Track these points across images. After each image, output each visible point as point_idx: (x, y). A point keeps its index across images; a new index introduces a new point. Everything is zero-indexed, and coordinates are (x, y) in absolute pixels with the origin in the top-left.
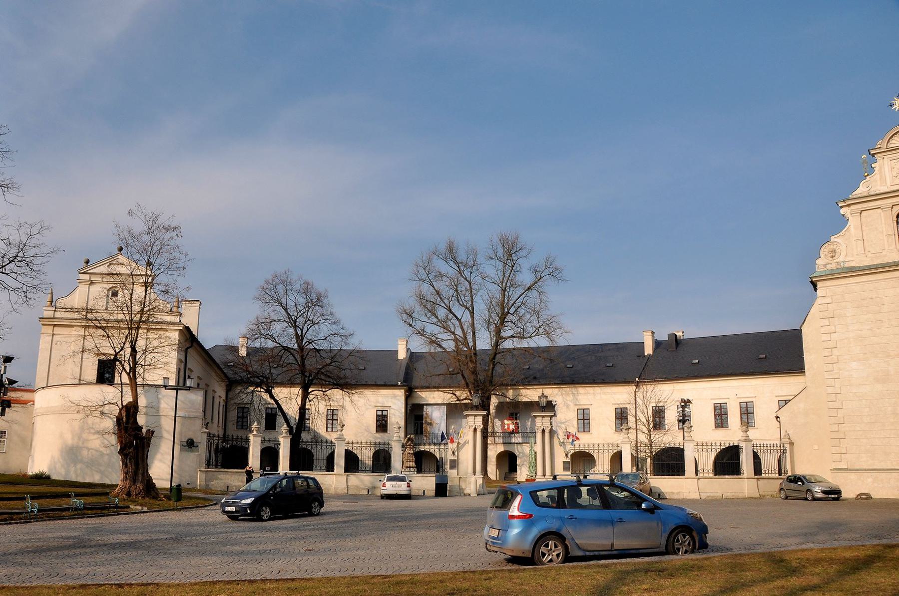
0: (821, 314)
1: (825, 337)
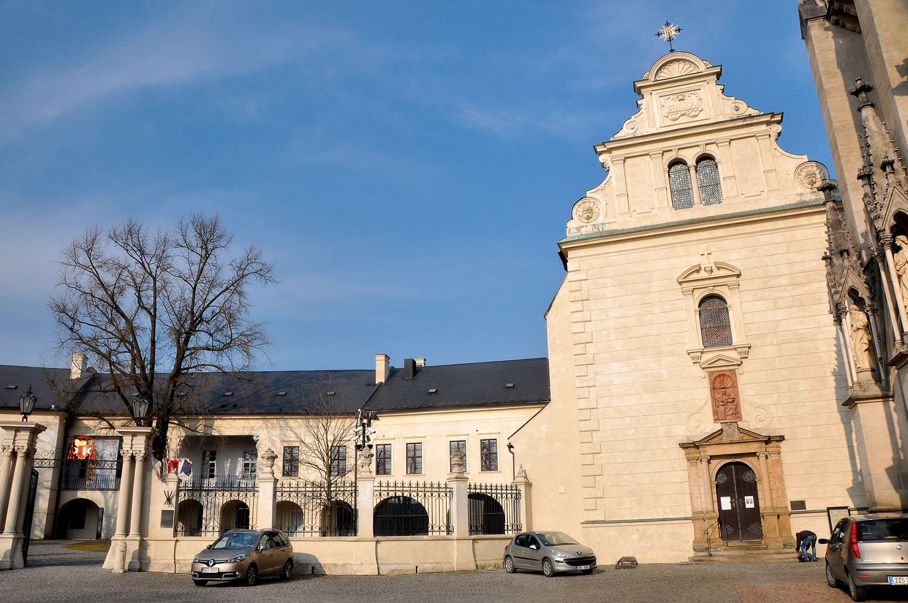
0: (573, 294)
1: (577, 328)
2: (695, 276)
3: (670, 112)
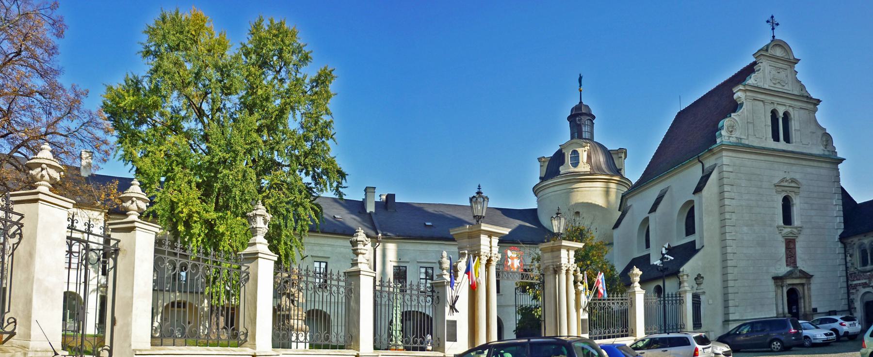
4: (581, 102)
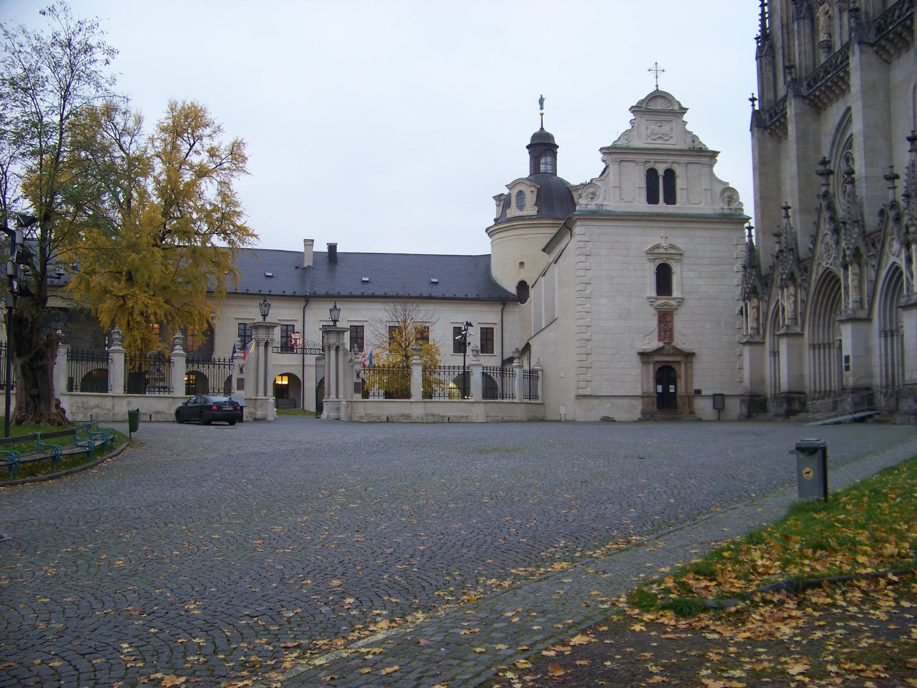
2: (657, 251)
3: (652, 134)
4: (542, 129)
